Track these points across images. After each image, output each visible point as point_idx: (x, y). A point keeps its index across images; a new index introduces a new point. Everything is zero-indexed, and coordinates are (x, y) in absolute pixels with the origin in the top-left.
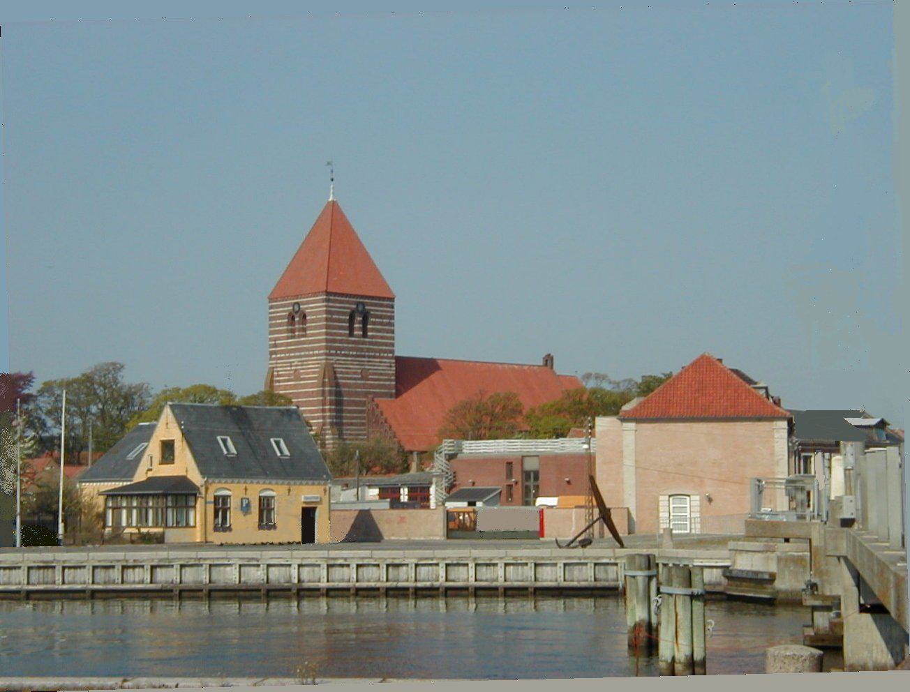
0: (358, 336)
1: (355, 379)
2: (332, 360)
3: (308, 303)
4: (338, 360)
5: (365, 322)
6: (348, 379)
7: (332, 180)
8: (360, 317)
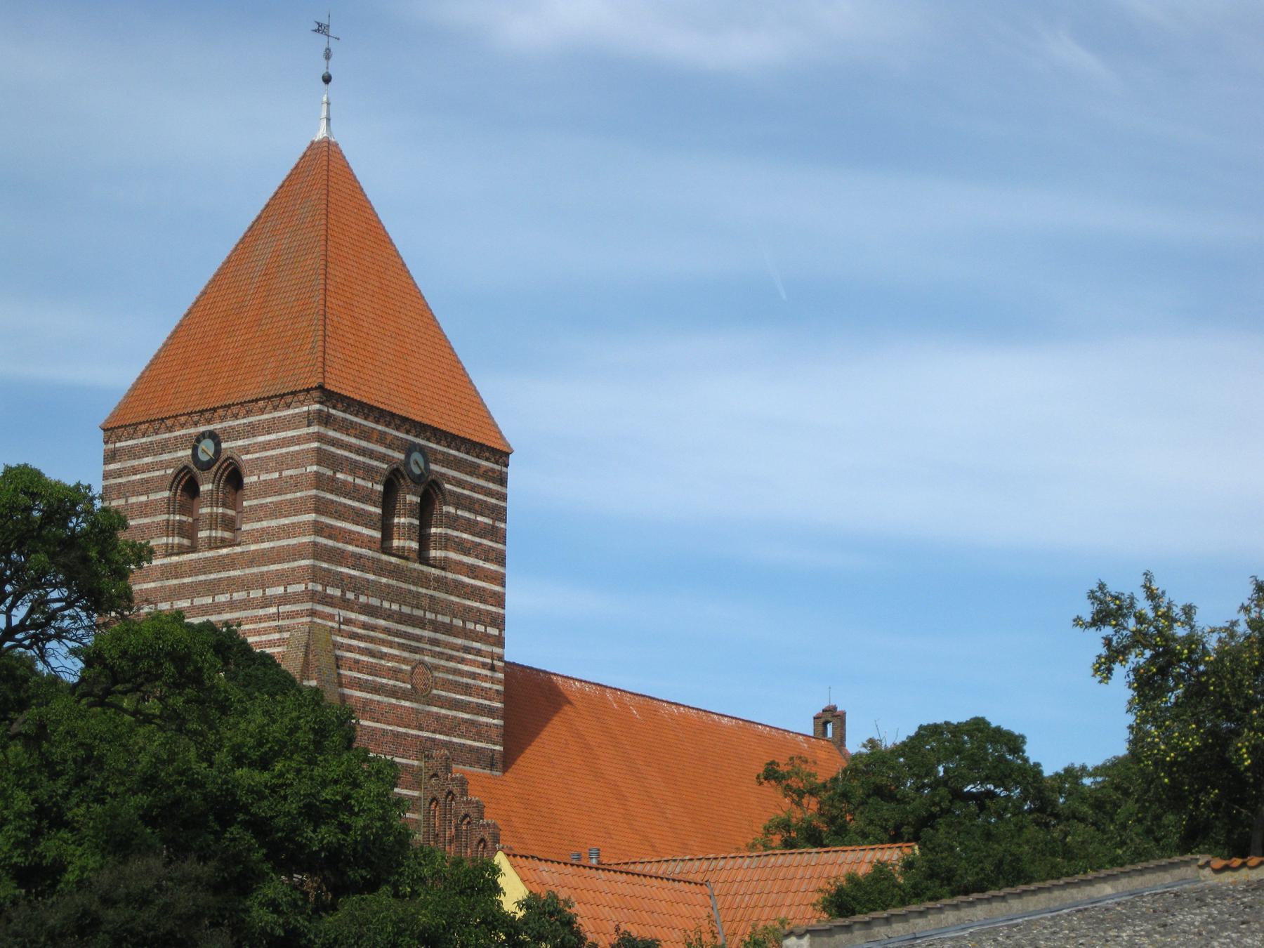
0: (402, 554)
1: (393, 693)
2: (331, 617)
3: (252, 430)
4: (348, 622)
5: (425, 512)
6: (376, 689)
7: (327, 79)
8: (414, 494)
